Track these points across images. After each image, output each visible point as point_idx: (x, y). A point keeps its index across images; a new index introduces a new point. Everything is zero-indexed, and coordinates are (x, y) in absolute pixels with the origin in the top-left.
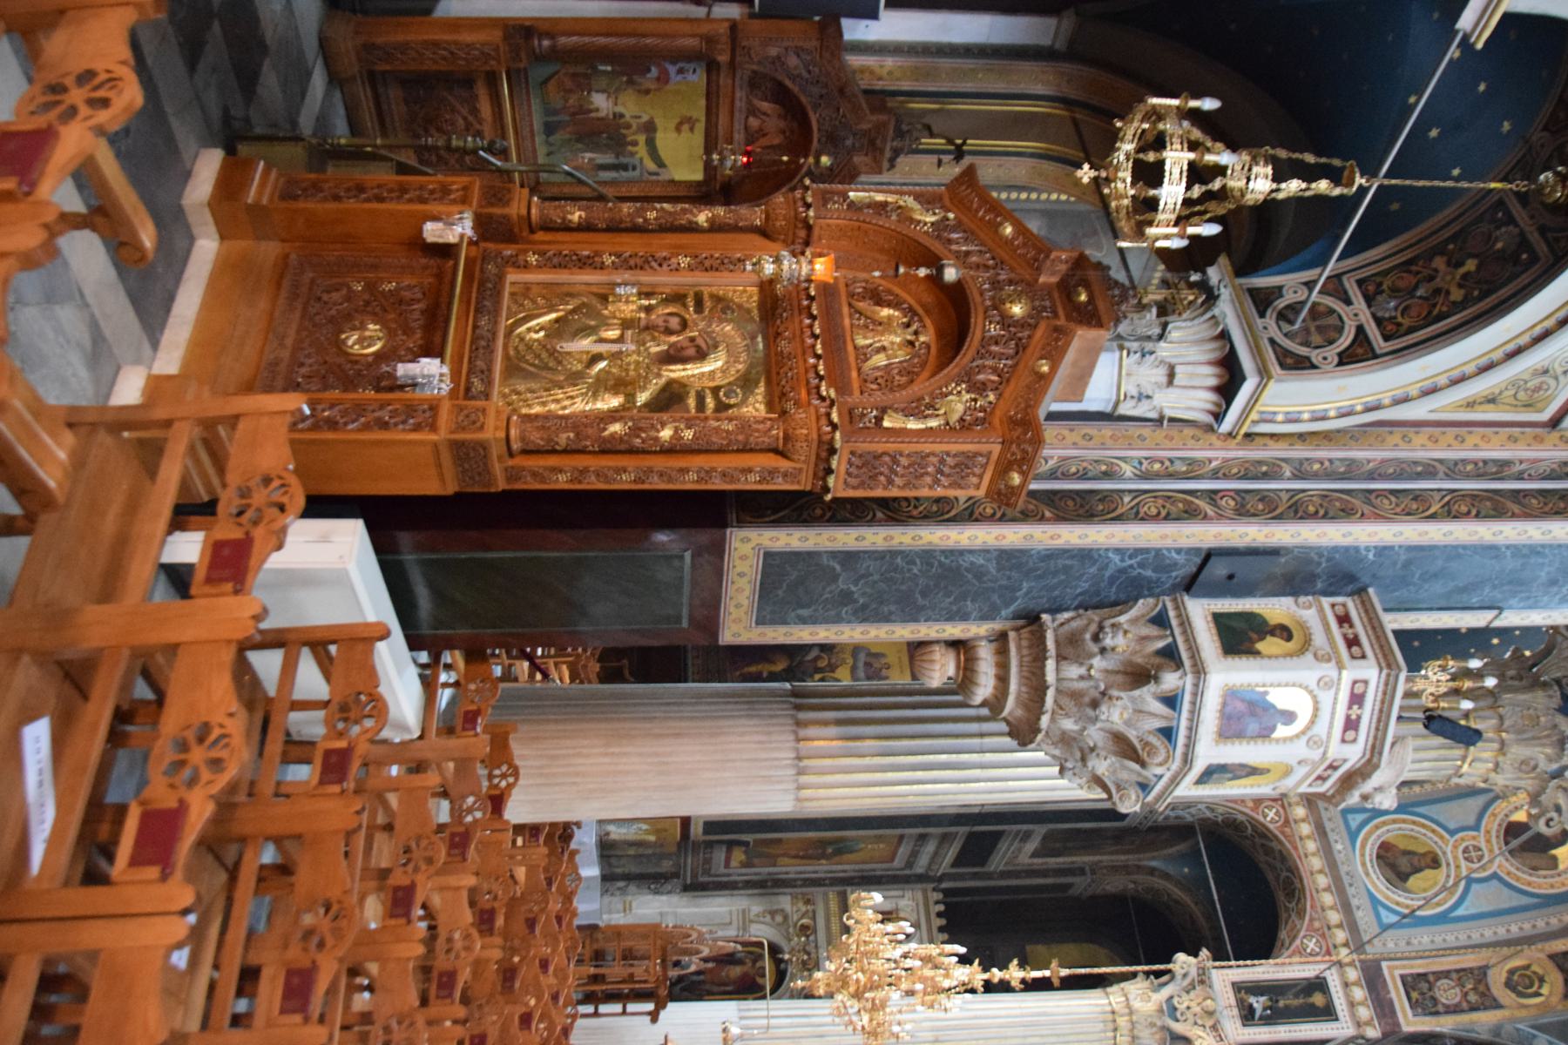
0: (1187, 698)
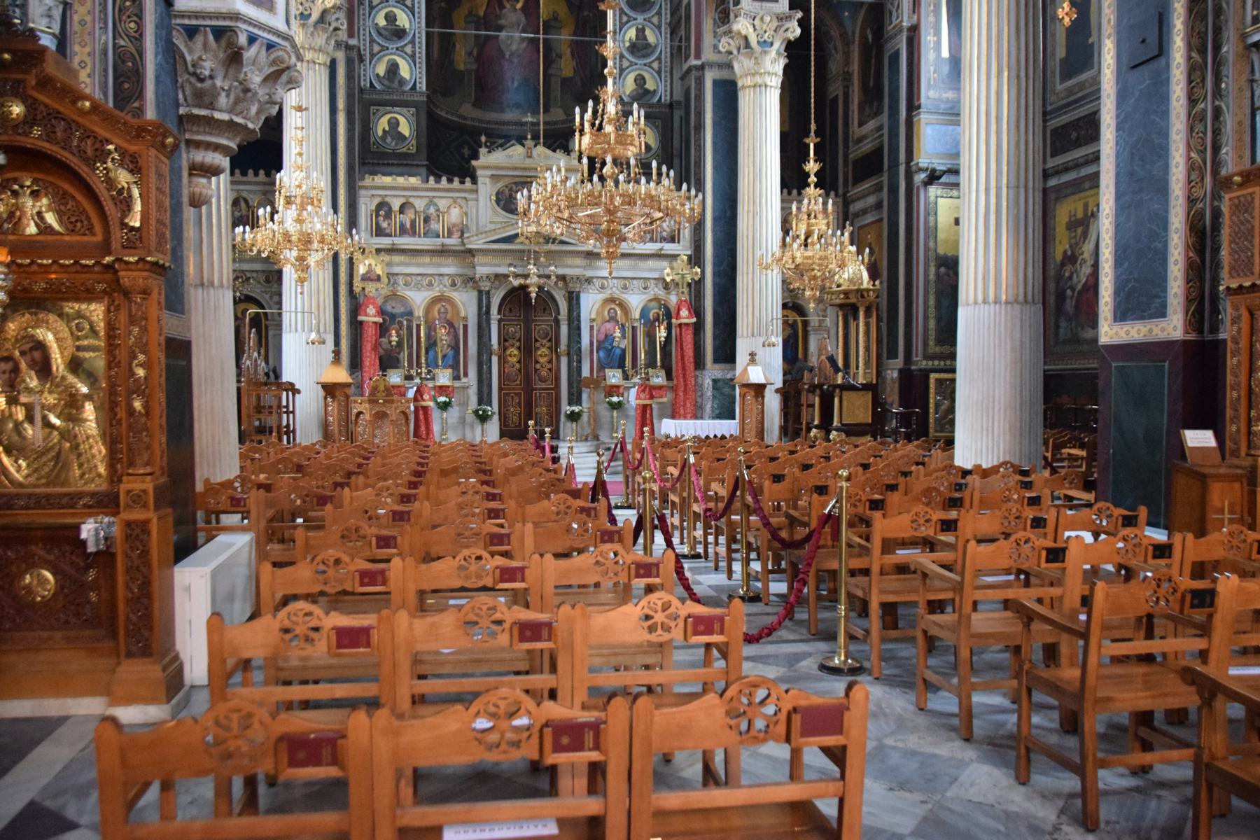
0: (251, 29)
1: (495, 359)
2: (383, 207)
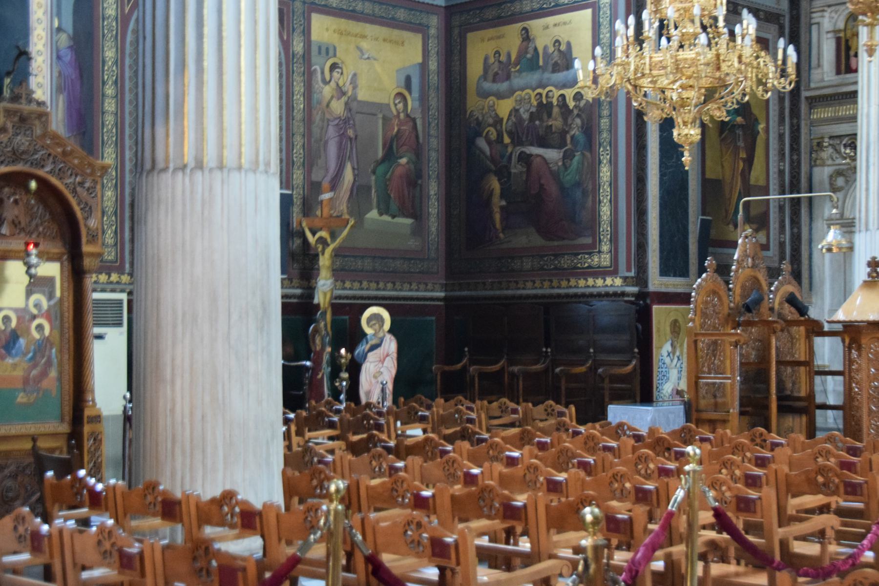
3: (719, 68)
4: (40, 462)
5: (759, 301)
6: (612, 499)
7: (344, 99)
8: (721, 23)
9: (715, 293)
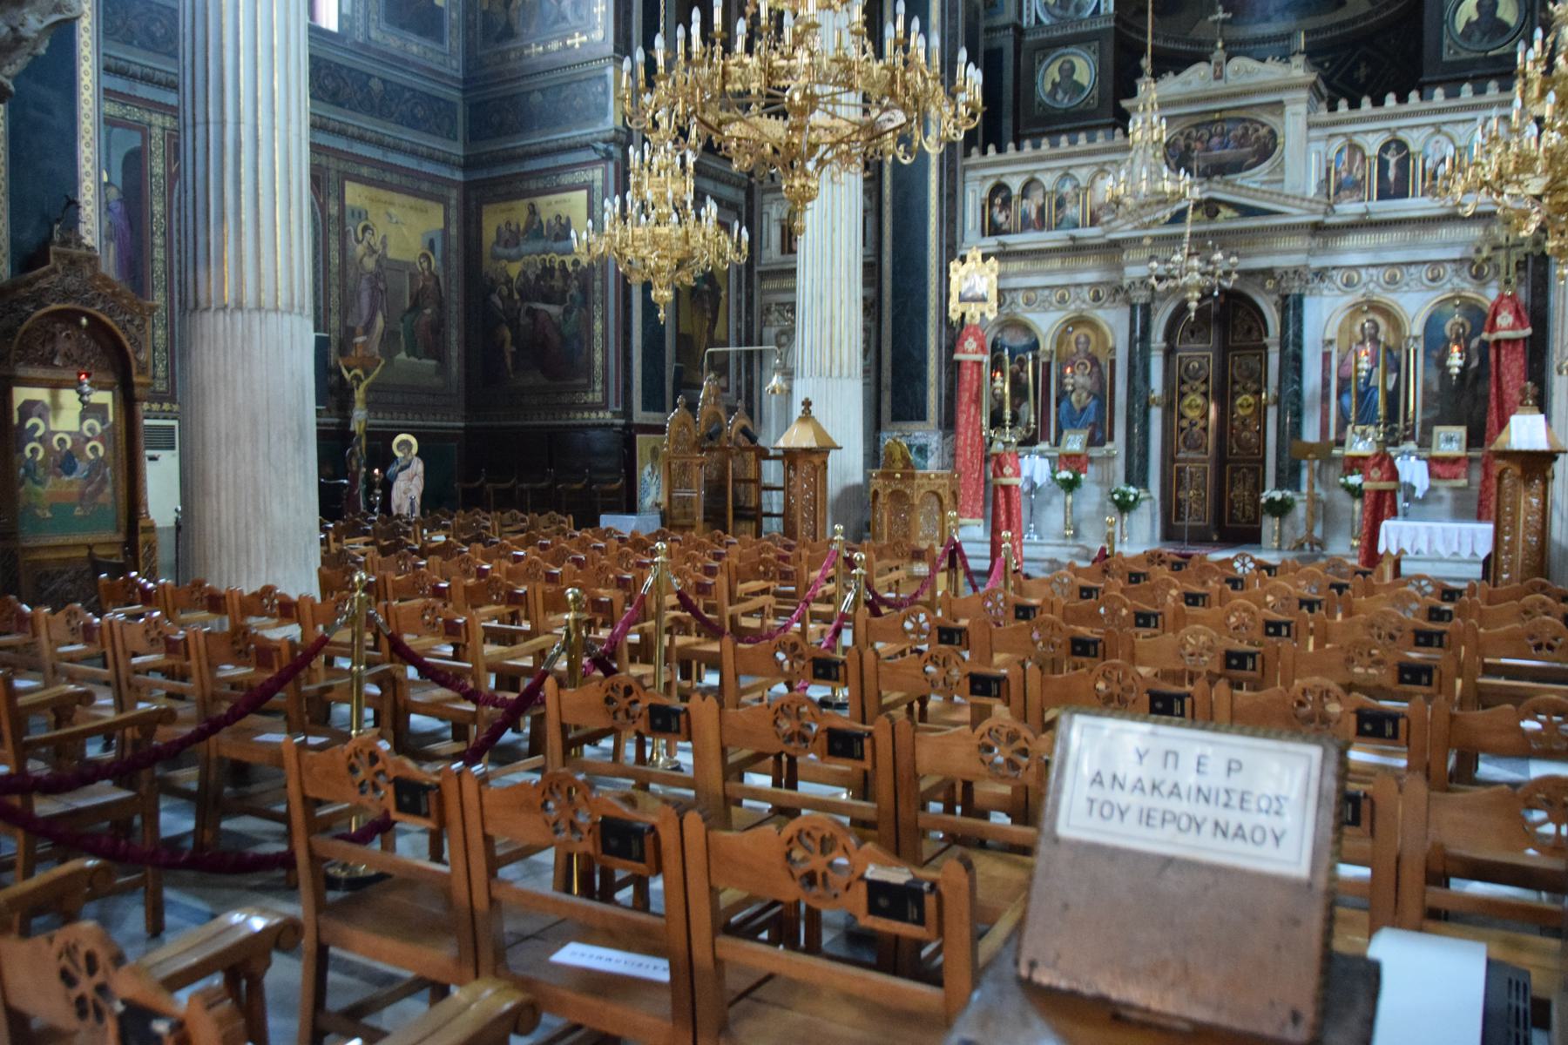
1: (1156, 414)
2: (999, 188)
3: (687, 242)
4: (97, 566)
5: (720, 431)
6: (599, 587)
7: (375, 257)
8: (689, 206)
9: (685, 425)
